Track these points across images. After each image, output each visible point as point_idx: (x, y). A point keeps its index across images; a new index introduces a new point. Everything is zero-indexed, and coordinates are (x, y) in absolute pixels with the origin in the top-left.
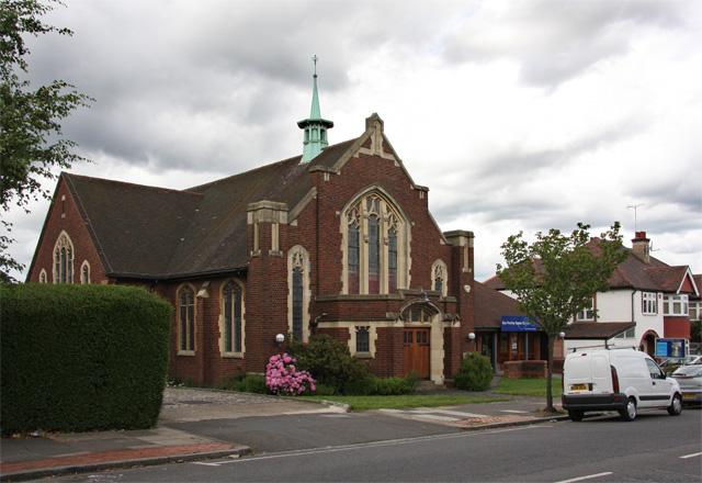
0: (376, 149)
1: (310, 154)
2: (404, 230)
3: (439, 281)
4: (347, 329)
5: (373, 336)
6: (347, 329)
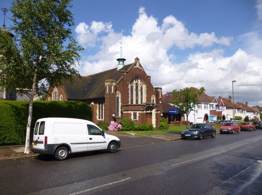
0: (138, 66)
1: (120, 67)
2: (144, 87)
3: (153, 100)
4: (131, 113)
5: (138, 115)
6: (131, 113)
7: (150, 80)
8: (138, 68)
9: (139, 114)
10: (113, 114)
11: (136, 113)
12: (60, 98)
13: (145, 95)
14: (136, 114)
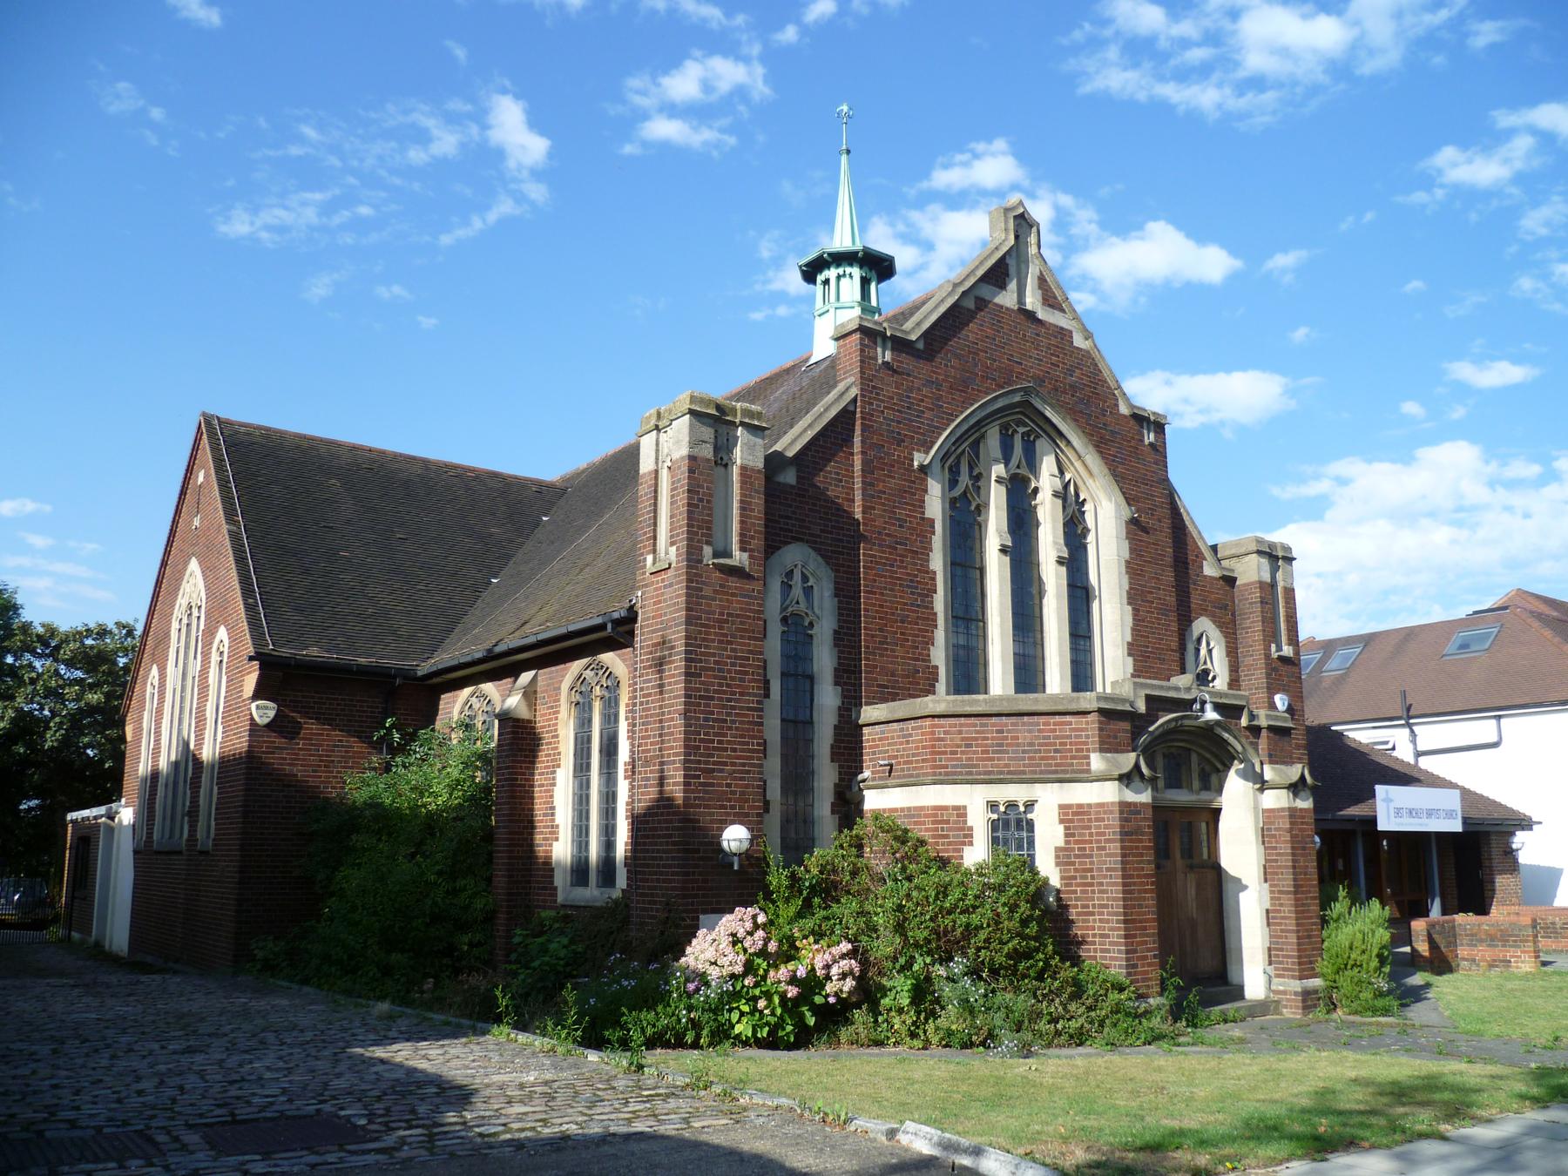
2: (1107, 517)
4: (961, 812)
6: (961, 812)
7: (1159, 450)
8: (1030, 316)
9: (1072, 816)
10: (725, 823)
11: (1030, 805)
12: (215, 658)
13: (1112, 620)
14: (1030, 825)
